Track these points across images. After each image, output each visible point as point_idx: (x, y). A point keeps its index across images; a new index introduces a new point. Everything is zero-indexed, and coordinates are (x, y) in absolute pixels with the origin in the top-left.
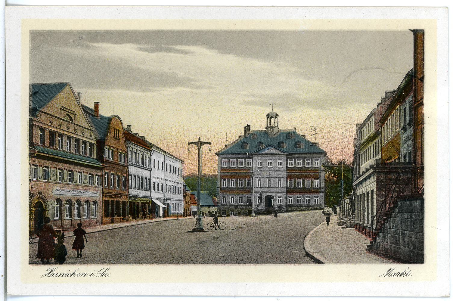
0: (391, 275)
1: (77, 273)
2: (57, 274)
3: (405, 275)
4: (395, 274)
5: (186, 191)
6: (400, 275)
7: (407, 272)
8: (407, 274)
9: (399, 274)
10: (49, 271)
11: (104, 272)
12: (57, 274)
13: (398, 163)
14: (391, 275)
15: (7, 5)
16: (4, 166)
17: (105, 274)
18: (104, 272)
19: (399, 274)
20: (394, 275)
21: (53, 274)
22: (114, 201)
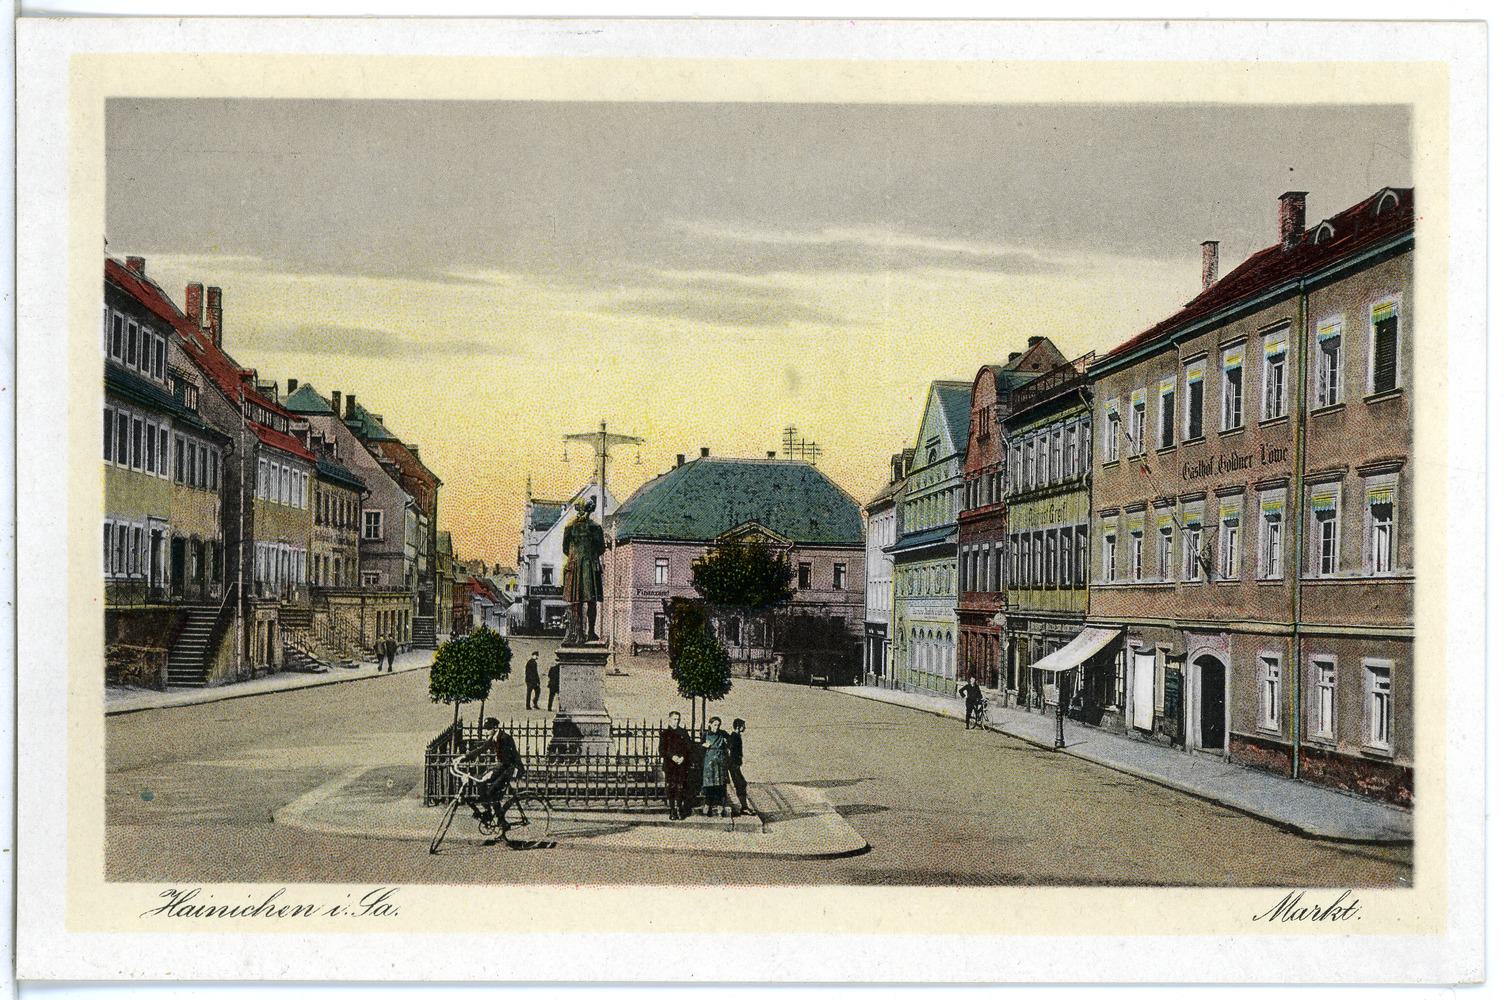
0: (1292, 917)
1: (279, 904)
2: (1271, 919)
3: (1337, 916)
4: (1303, 912)
5: (1278, 415)
6: (1320, 915)
7: (1345, 904)
8: (1345, 913)
9: (1317, 914)
10: (169, 899)
11: (379, 900)
12: (1271, 919)
13: (334, 588)
14: (1292, 917)
15: (19, 13)
16: (12, 684)
17: (1300, 912)
18: (379, 900)
19: (1317, 914)
20: (1300, 917)
21: (386, 907)
22: (1056, 530)
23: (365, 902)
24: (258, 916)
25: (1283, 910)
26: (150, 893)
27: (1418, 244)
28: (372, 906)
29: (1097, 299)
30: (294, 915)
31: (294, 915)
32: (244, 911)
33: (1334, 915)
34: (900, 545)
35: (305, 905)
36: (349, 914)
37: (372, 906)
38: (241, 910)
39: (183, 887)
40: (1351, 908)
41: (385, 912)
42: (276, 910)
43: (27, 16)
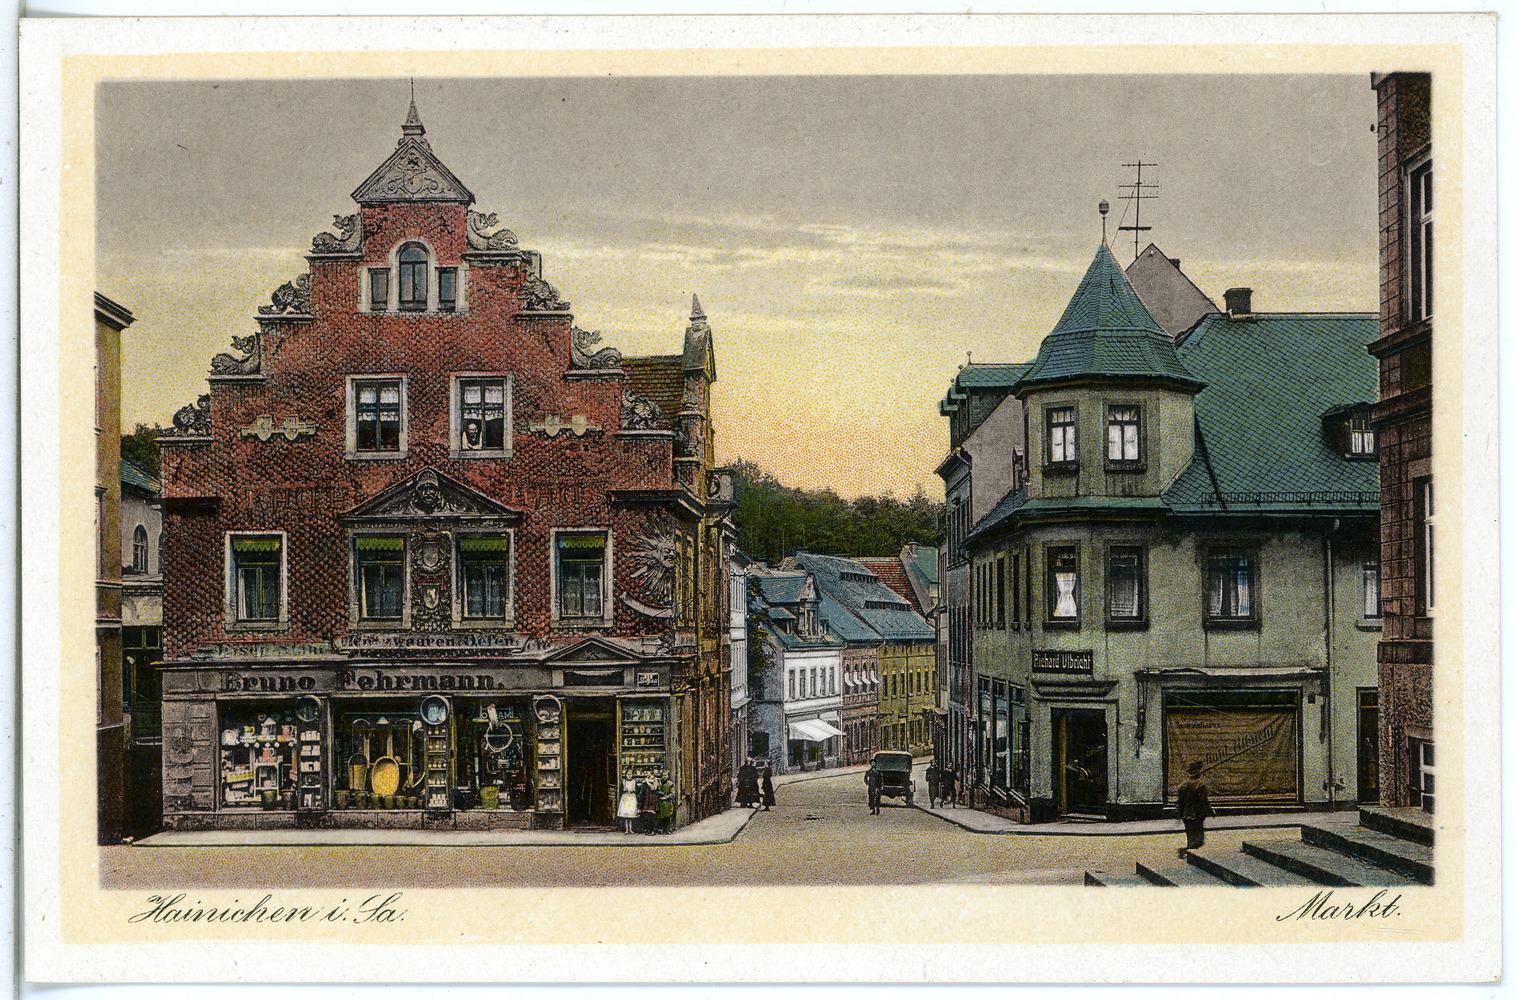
4: (1336, 910)
7: (1384, 901)
10: (155, 905)
23: (368, 906)
24: (292, 920)
25: (160, 910)
26: (139, 899)
27: (1434, 145)
28: (377, 909)
29: (322, 373)
30: (194, 920)
31: (194, 920)
32: (224, 914)
33: (1372, 912)
34: (952, 485)
35: (301, 908)
36: (350, 920)
37: (377, 909)
38: (298, 916)
39: (167, 894)
40: (1391, 905)
41: (1332, 914)
42: (269, 913)
43: (100, 341)
